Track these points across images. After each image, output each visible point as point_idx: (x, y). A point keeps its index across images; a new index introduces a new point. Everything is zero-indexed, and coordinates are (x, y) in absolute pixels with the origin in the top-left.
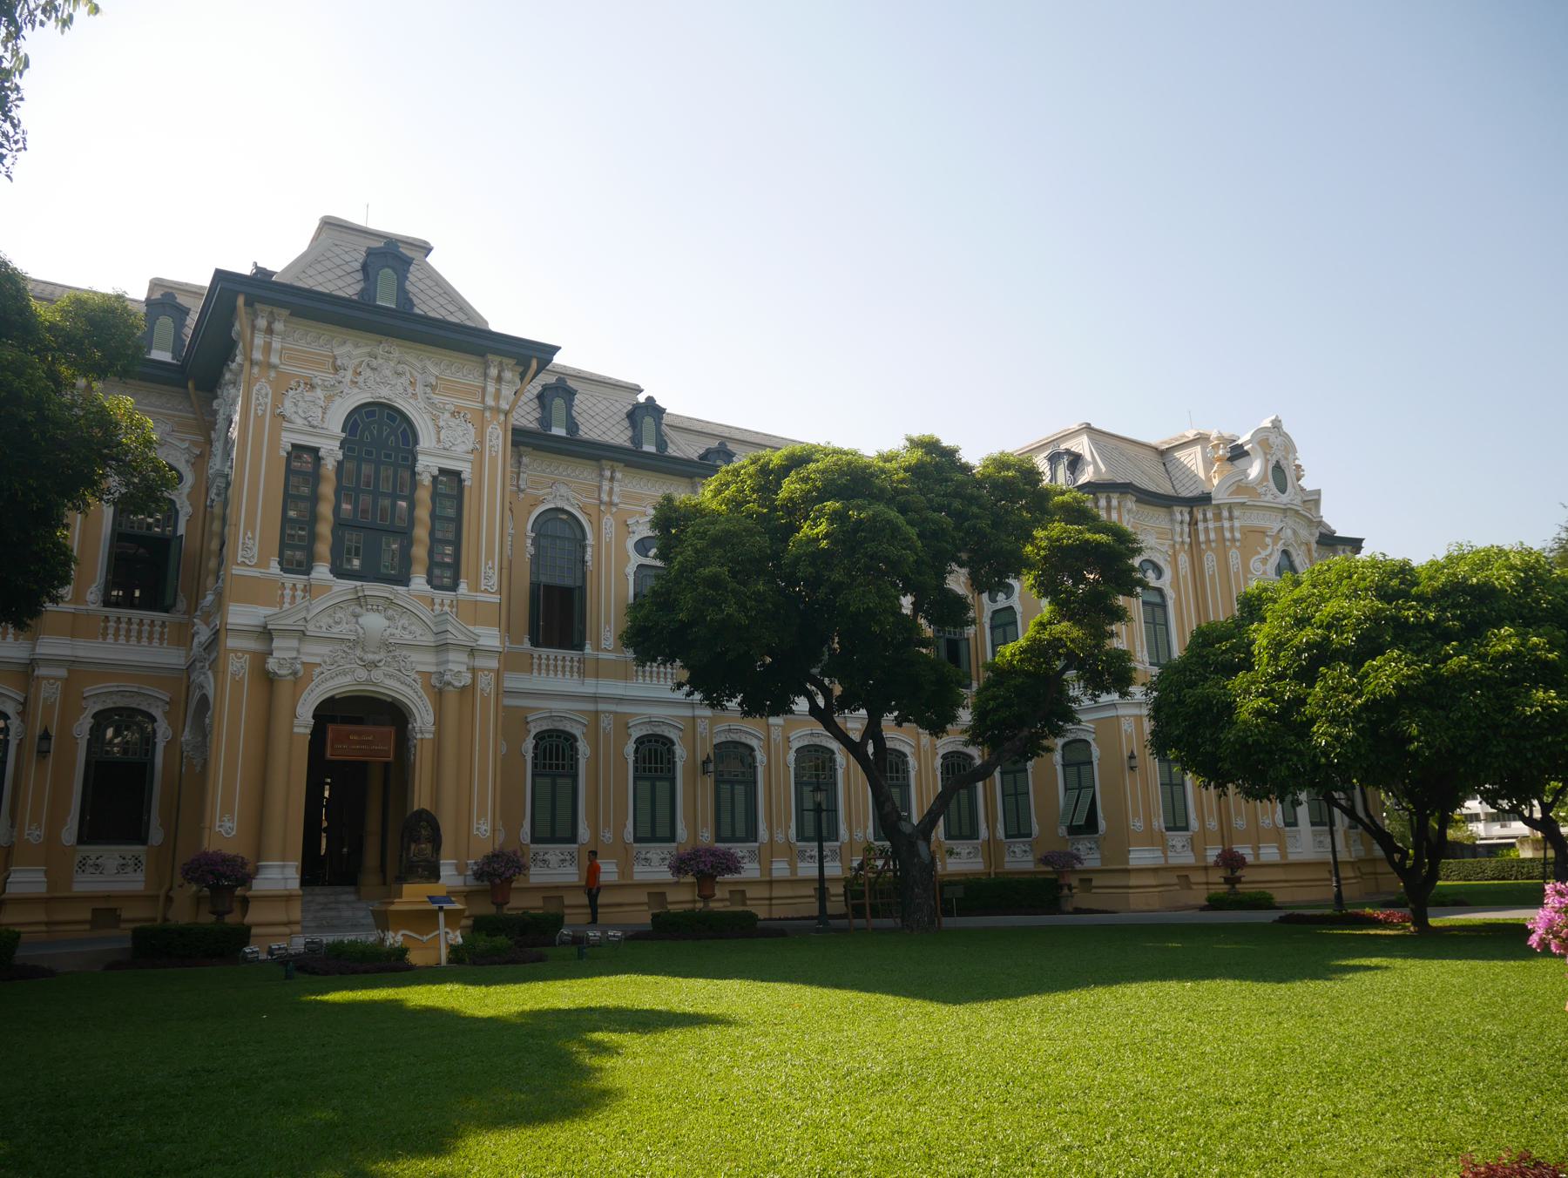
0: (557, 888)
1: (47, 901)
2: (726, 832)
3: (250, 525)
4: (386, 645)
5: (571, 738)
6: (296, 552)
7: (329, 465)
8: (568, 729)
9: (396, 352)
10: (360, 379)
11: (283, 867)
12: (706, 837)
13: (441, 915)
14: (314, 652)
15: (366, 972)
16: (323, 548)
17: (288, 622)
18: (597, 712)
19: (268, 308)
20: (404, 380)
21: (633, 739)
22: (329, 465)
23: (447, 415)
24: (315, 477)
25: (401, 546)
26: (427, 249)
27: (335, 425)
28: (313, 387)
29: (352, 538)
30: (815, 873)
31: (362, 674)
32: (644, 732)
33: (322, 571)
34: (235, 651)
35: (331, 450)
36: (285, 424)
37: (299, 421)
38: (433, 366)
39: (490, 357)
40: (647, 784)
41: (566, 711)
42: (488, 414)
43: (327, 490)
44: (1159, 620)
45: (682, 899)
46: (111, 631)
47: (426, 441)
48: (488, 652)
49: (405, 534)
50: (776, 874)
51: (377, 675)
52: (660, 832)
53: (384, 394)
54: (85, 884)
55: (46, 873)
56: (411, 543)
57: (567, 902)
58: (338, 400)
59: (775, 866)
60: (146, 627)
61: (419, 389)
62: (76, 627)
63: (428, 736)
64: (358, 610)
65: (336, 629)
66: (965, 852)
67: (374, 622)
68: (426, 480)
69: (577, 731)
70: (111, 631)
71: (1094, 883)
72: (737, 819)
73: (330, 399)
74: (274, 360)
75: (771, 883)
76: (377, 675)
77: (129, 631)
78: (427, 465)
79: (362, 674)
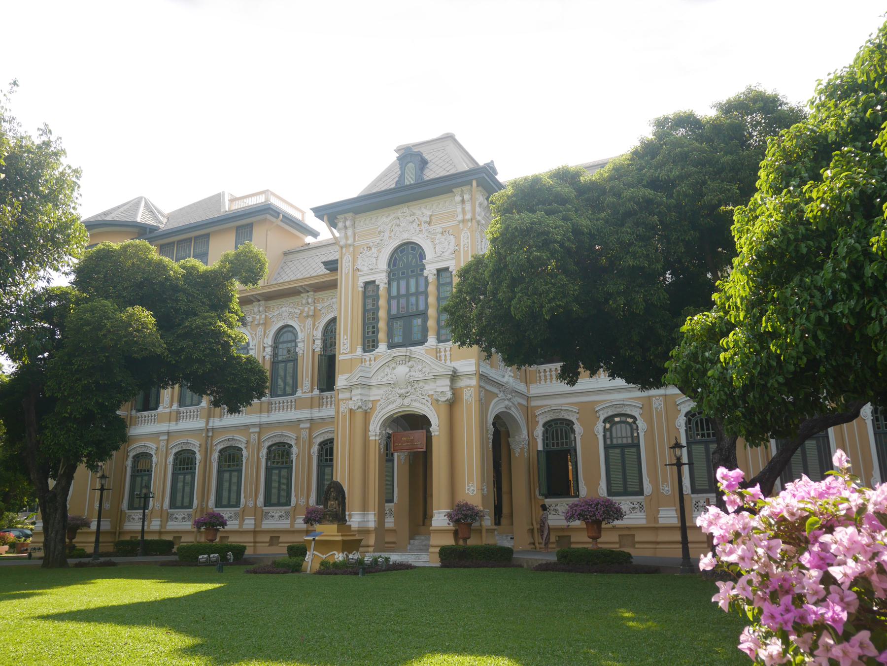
0: (177, 532)
1: (255, 532)
2: (618, 486)
3: (346, 333)
4: (411, 383)
5: (570, 423)
6: (370, 344)
7: (383, 287)
8: (566, 417)
9: (405, 210)
10: (392, 234)
11: (364, 515)
12: (602, 490)
13: (313, 543)
14: (376, 394)
15: (278, 573)
16: (382, 335)
17: (354, 381)
18: (649, 397)
19: (459, 189)
20: (415, 225)
21: (602, 418)
22: (383, 287)
23: (439, 236)
24: (376, 298)
25: (422, 322)
26: (449, 138)
27: (383, 265)
28: (370, 248)
29: (398, 325)
30: (140, 528)
31: (399, 401)
32: (549, 418)
33: (382, 347)
34: (342, 400)
35: (381, 279)
36: (359, 273)
37: (365, 269)
38: (424, 210)
39: (454, 190)
40: (701, 448)
41: (562, 405)
42: (461, 225)
43: (382, 302)
44: (369, 301)
45: (581, 540)
46: (543, 378)
47: (429, 255)
48: (468, 375)
49: (424, 315)
50: (662, 522)
51: (407, 401)
52: (283, 501)
53: (405, 237)
54: (268, 524)
55: (255, 520)
56: (427, 319)
57: (637, 539)
58: (383, 250)
59: (662, 514)
60: (548, 373)
61: (424, 226)
62: (312, 404)
63: (437, 433)
64: (393, 365)
65: (385, 379)
66: (277, 515)
67: (402, 370)
68: (432, 279)
69: (636, 413)
70: (543, 378)
71: (281, 540)
72: (228, 495)
73: (379, 251)
74: (350, 242)
75: (657, 529)
76: (407, 401)
77: (545, 376)
78: (430, 270)
79: (399, 401)
